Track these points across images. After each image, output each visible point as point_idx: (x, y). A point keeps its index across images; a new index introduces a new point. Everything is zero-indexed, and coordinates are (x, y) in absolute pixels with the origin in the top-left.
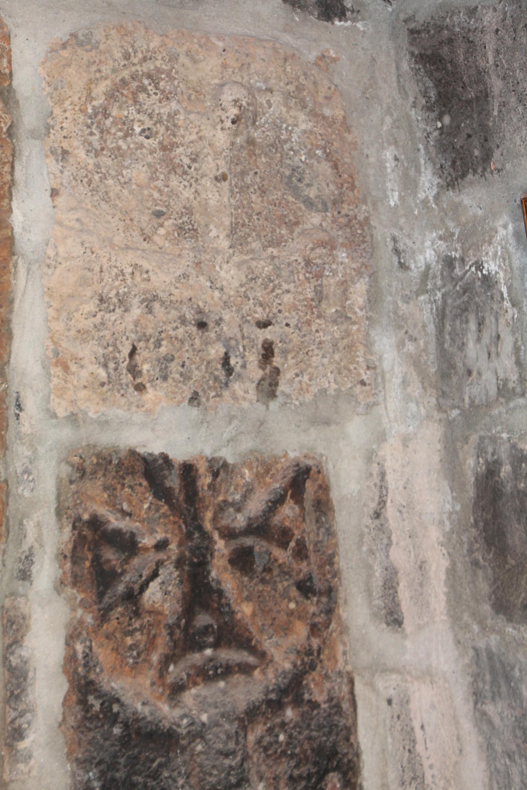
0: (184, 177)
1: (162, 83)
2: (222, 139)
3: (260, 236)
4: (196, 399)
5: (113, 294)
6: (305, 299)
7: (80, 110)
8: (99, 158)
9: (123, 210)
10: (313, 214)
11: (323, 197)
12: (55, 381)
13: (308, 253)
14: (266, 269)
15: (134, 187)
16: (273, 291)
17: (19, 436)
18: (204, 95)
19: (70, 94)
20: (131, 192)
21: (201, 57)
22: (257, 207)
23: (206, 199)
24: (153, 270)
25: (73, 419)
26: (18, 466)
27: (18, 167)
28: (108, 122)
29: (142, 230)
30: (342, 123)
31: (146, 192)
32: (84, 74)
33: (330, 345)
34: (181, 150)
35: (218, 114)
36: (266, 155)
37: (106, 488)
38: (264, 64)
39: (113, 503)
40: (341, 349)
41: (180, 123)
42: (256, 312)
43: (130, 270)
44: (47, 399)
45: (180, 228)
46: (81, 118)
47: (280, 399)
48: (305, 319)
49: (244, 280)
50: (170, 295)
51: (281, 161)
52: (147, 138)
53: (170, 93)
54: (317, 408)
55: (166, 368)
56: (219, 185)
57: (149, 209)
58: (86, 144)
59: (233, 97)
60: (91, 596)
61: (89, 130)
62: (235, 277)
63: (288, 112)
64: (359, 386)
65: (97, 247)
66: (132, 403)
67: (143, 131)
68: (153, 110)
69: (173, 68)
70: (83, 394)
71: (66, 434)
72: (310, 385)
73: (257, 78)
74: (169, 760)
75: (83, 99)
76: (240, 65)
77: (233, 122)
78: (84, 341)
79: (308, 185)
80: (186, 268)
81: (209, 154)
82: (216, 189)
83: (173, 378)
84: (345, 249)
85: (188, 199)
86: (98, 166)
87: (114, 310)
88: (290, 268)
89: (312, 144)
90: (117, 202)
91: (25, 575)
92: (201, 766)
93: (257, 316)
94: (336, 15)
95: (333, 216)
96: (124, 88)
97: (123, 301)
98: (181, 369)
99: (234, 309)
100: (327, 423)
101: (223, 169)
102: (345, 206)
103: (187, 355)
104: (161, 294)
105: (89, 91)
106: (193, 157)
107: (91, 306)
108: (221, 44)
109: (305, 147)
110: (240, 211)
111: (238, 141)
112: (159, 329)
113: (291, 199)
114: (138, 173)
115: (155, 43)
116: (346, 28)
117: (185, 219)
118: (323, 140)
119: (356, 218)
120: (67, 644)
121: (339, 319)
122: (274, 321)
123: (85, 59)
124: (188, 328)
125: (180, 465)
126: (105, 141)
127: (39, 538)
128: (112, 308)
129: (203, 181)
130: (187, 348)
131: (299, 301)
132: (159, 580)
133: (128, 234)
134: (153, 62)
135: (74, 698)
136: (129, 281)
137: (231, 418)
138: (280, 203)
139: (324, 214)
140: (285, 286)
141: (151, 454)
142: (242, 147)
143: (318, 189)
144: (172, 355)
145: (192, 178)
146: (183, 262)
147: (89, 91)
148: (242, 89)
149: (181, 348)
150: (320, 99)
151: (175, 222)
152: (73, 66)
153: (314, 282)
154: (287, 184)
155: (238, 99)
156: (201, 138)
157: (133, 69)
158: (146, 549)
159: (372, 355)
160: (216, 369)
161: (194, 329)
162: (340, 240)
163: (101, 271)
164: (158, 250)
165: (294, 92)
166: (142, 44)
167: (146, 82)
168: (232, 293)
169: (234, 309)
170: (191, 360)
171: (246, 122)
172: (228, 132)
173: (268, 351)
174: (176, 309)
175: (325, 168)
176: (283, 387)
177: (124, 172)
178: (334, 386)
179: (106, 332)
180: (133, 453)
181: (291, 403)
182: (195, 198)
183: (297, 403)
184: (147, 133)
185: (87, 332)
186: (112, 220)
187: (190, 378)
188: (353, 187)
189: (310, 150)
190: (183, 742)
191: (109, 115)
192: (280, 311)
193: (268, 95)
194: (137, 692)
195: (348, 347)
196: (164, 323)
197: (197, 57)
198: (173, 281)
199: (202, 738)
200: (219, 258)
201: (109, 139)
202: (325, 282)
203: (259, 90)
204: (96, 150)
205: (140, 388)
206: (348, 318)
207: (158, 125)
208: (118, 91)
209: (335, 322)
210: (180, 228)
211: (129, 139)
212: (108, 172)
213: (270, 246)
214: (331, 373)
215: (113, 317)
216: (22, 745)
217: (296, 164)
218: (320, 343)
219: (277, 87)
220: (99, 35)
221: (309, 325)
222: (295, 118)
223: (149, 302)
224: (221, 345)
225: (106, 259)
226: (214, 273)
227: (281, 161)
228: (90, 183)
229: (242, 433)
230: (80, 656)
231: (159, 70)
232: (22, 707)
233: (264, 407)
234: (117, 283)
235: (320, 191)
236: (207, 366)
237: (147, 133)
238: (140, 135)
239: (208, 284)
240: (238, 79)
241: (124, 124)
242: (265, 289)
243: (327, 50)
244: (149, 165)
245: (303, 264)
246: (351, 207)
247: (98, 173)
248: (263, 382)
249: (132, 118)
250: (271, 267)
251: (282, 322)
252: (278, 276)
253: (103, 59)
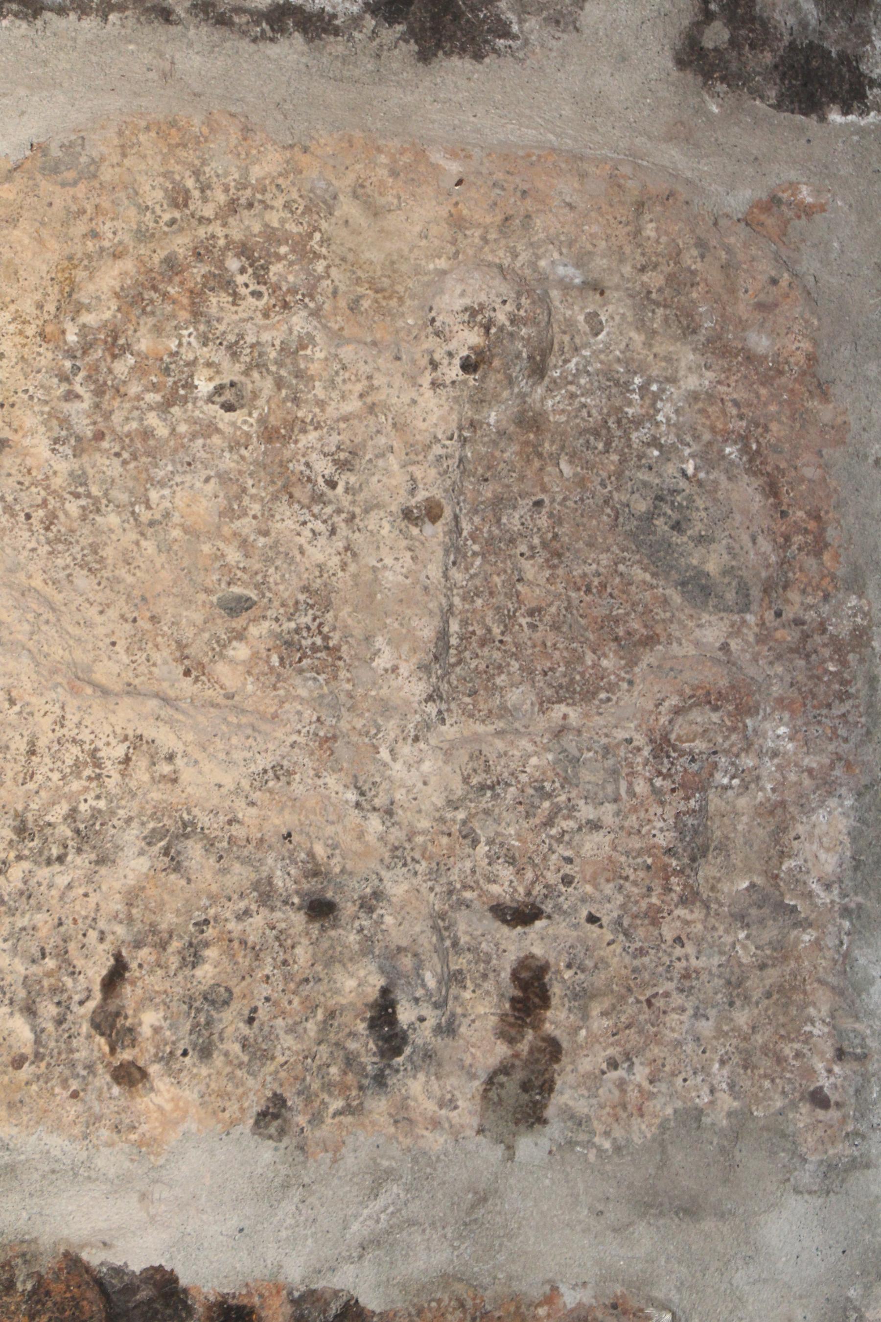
0: (316, 509)
1: (276, 269)
2: (433, 412)
3: (532, 672)
4: (276, 1116)
6: (649, 850)
7: (42, 335)
8: (85, 458)
9: (136, 593)
10: (705, 617)
11: (744, 573)
13: (664, 720)
14: (534, 761)
15: (176, 533)
16: (549, 822)
18: (401, 300)
19: (14, 293)
20: (165, 548)
21: (390, 199)
22: (531, 595)
23: (374, 569)
24: (185, 754)
28: (122, 367)
29: (181, 646)
30: (804, 373)
31: (206, 548)
32: (53, 244)
33: (719, 982)
34: (313, 436)
35: (425, 346)
36: (573, 457)
38: (571, 216)
40: (756, 995)
41: (314, 368)
42: (492, 879)
43: (120, 751)
45: (289, 644)
46: (46, 357)
47: (555, 1130)
48: (644, 905)
49: (458, 788)
50: (230, 823)
51: (619, 475)
52: (229, 407)
53: (293, 291)
54: (663, 1164)
55: (209, 1023)
56: (415, 531)
57: (208, 591)
58: (55, 422)
59: (467, 301)
61: (64, 387)
62: (433, 780)
63: (648, 345)
64: (805, 1108)
65: (28, 686)
66: (99, 1118)
67: (219, 390)
68: (241, 336)
69: (316, 229)
72: (652, 1096)
73: (556, 255)
75: (51, 307)
76: (499, 218)
77: (468, 366)
79: (700, 540)
80: (285, 750)
81: (391, 449)
82: (405, 543)
83: (226, 1054)
84: (786, 716)
85: (320, 567)
86: (79, 479)
87: (61, 859)
88: (610, 762)
89: (713, 429)
90: (122, 572)
93: (495, 889)
94: (834, 98)
95: (762, 624)
96: (170, 280)
97: (90, 836)
98: (245, 1030)
99: (422, 867)
100: (690, 1210)
101: (432, 488)
102: (794, 595)
103: (265, 990)
104: (204, 820)
105: (69, 290)
106: (342, 456)
108: (454, 168)
109: (697, 438)
110: (479, 602)
111: (492, 420)
112: (199, 916)
113: (639, 574)
114: (192, 498)
115: (268, 165)
116: (862, 132)
117: (305, 620)
118: (741, 417)
119: (824, 631)
121: (753, 911)
122: (548, 907)
123: (58, 203)
124: (278, 915)
125: (210, 1308)
126: (107, 416)
128: (55, 851)
129: (372, 521)
130: (268, 970)
131: (627, 854)
133: (141, 657)
134: (261, 216)
136: (112, 783)
137: (380, 1179)
138: (603, 586)
139: (736, 618)
140: (587, 812)
141: (118, 1271)
142: (502, 433)
143: (730, 549)
144: (228, 989)
145: (339, 511)
146: (279, 734)
147: (69, 290)
148: (497, 281)
149: (251, 972)
150: (743, 310)
151: (275, 626)
152: (23, 223)
153: (676, 803)
154: (632, 535)
155: (482, 307)
156: (372, 409)
157: (202, 232)
159: (857, 1018)
160: (352, 1035)
161: (299, 919)
162: (776, 690)
163: (32, 752)
164: (221, 700)
165: (660, 290)
166: (222, 166)
167: (233, 264)
168: (424, 824)
169: (422, 867)
170: (276, 1004)
171: (507, 366)
172: (452, 392)
173: (530, 991)
174: (246, 861)
175: (747, 493)
176: (567, 1096)
177: (154, 495)
178: (727, 1102)
179: (40, 918)
180: (72, 1262)
181: (589, 1144)
182: (344, 566)
183: (607, 1145)
184: (228, 395)
186: (99, 619)
187: (266, 1056)
188: (819, 546)
189: (710, 444)
191: (127, 348)
192: (567, 881)
193: (593, 302)
195: (781, 990)
196: (213, 899)
197: (381, 201)
198: (245, 784)
200: (391, 727)
202: (715, 802)
203: (565, 286)
204: (79, 439)
205: (130, 1076)
206: (783, 909)
207: (256, 375)
208: (154, 288)
209: (741, 918)
210: (289, 644)
211: (175, 410)
212: (106, 494)
213: (560, 701)
214: (723, 1062)
217: (669, 483)
218: (686, 976)
219: (616, 279)
220: (103, 144)
221: (655, 922)
222: (668, 359)
223: (172, 839)
224: (373, 967)
225: (50, 719)
226: (372, 768)
227: (619, 475)
229: (412, 1223)
231: (271, 235)
233: (499, 1151)
234: (76, 785)
235: (734, 556)
236: (325, 1026)
237: (230, 397)
238: (210, 400)
239: (351, 796)
240: (502, 257)
241: (167, 371)
242: (528, 816)
243: (793, 186)
244: (224, 478)
245: (646, 752)
246: (810, 600)
247: (77, 496)
248: (502, 1078)
249: (191, 357)
250: (550, 757)
251: (575, 909)
252: (566, 781)
253: (106, 204)
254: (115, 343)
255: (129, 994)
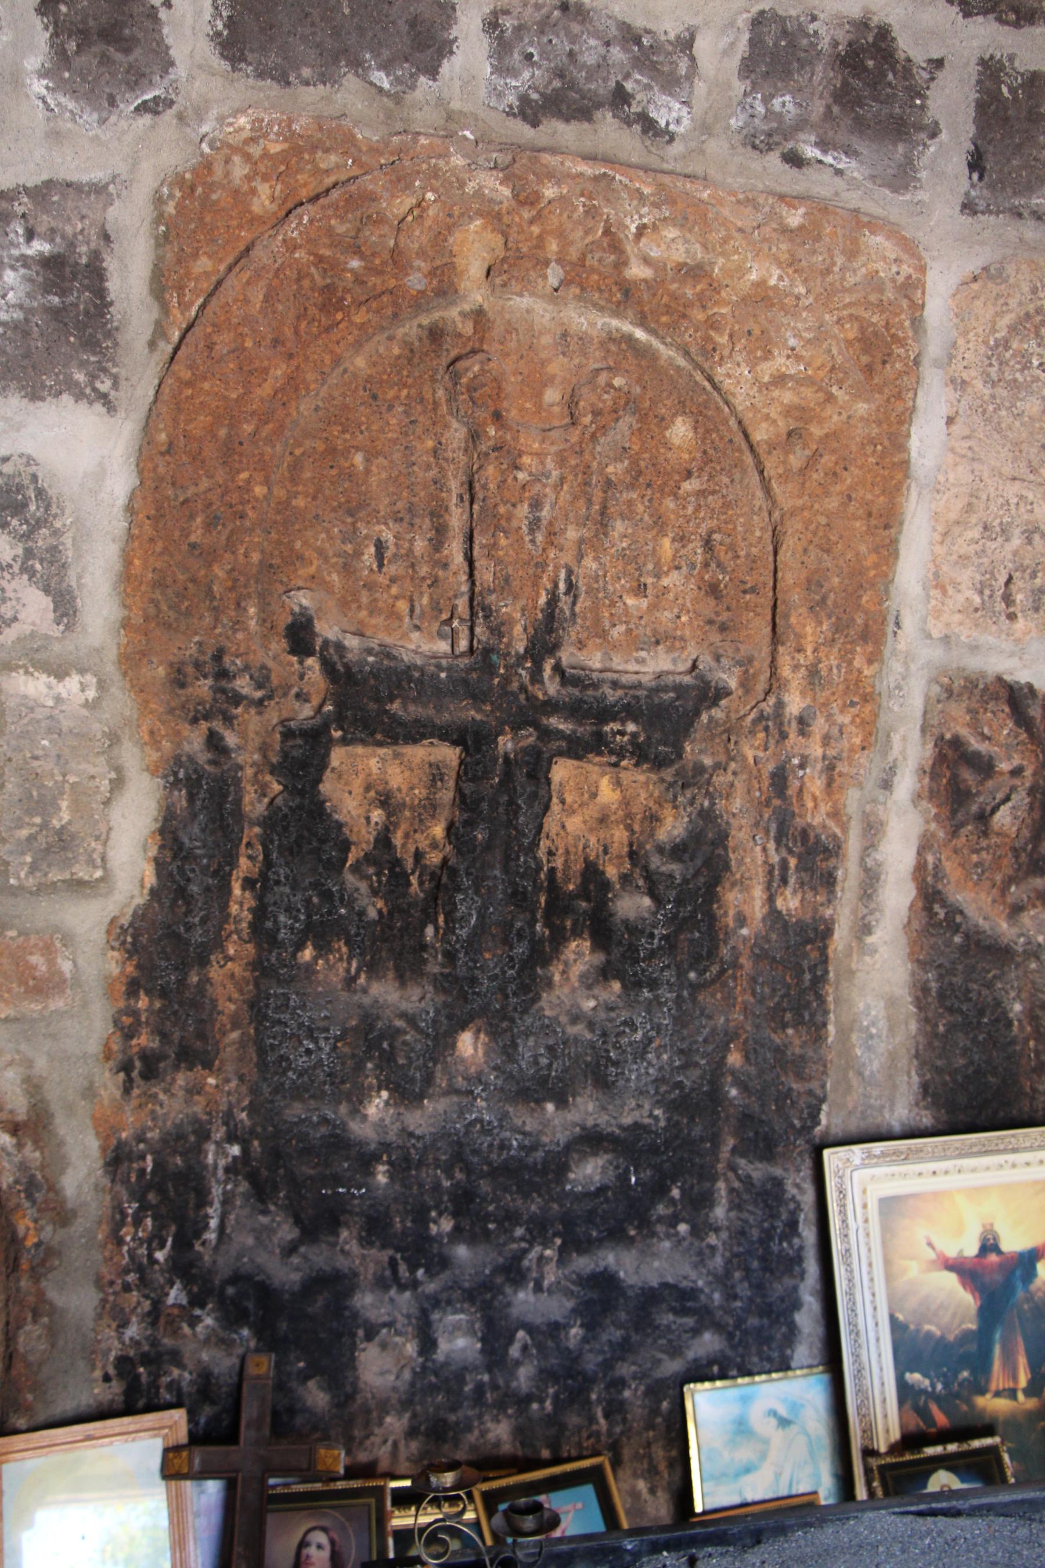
5: (996, 523)
12: (933, 602)
17: (894, 652)
25: (946, 640)
26: (892, 680)
27: (920, 394)
28: (1008, 355)
37: (969, 711)
39: (975, 725)
44: (924, 621)
46: (983, 349)
60: (946, 812)
70: (957, 617)
71: (936, 654)
74: (1003, 974)
78: (965, 566)
86: (993, 397)
91: (887, 785)
92: (1033, 983)
105: (994, 323)
107: (975, 533)
120: (919, 853)
127: (903, 752)
132: (1010, 804)
135: (920, 904)
136: (1013, 511)
158: (1001, 773)
180: (999, 679)
185: (967, 558)
190: (1019, 959)
194: (977, 905)
199: (1038, 958)
201: (1007, 370)
215: (993, 545)
216: (869, 940)
228: (984, 412)
230: (930, 867)
232: (872, 906)
254: (1006, 344)
255: (1013, 588)
